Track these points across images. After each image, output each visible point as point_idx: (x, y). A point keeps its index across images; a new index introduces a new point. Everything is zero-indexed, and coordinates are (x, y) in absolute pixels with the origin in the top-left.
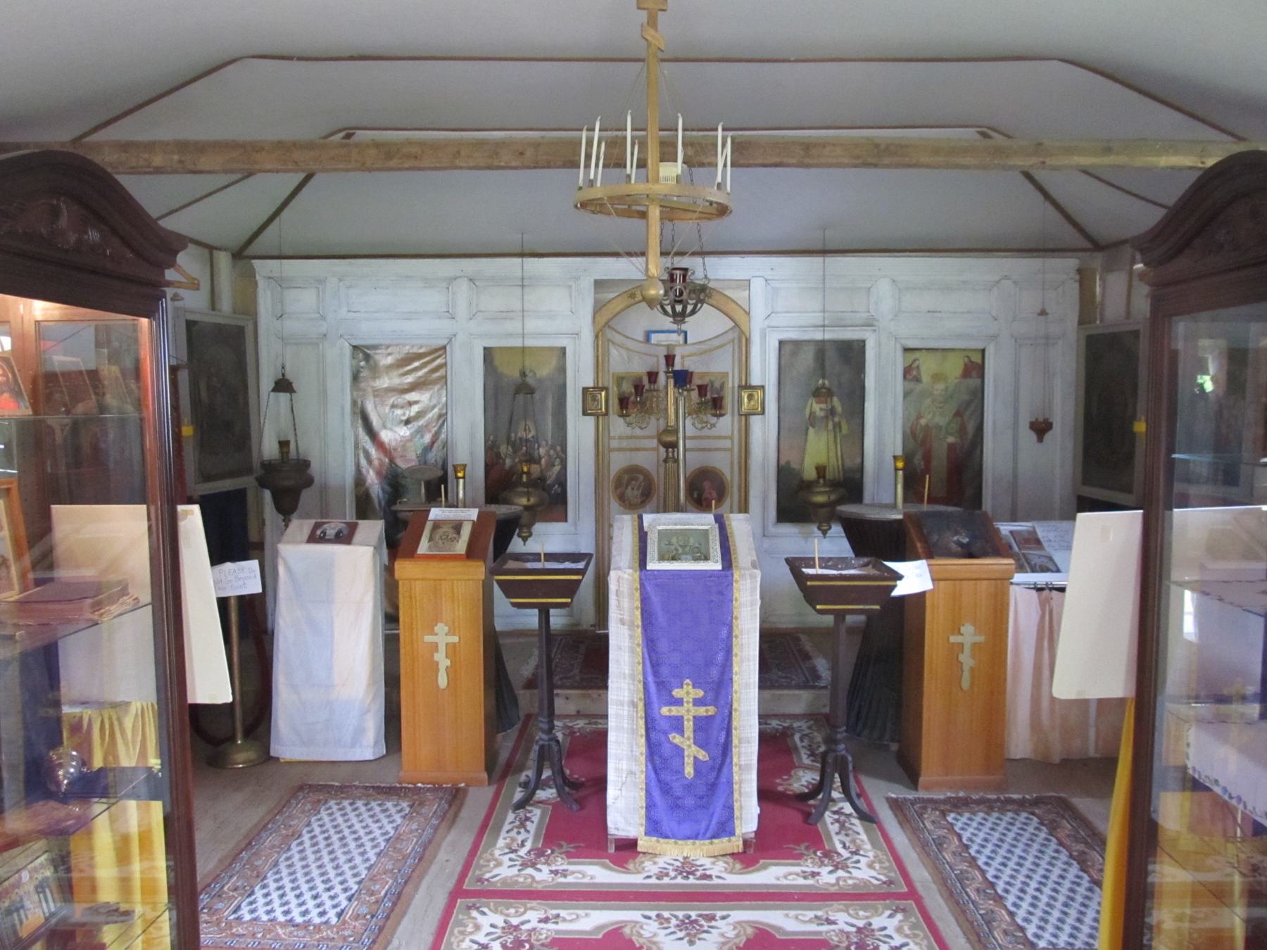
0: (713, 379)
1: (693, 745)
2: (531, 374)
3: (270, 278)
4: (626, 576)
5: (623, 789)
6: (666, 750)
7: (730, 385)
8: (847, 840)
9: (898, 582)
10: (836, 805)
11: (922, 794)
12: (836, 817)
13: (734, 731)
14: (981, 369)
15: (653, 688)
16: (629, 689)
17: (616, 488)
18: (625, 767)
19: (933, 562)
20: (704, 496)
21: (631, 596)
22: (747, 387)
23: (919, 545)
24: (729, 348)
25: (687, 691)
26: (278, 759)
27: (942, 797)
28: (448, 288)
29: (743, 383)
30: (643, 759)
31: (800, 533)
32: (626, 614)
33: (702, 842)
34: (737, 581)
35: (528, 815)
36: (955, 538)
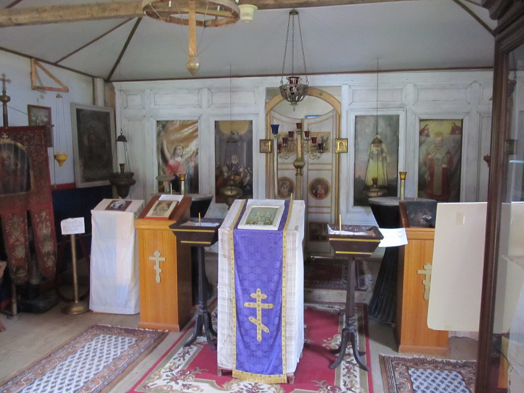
0: (323, 135)
1: (261, 324)
2: (236, 134)
3: (121, 90)
4: (226, 232)
5: (225, 344)
6: (247, 326)
7: (331, 138)
8: (348, 380)
9: (381, 240)
10: (350, 358)
11: (400, 355)
12: (348, 365)
13: (282, 318)
14: (461, 129)
15: (240, 292)
16: (228, 292)
17: (312, 191)
18: (226, 333)
19: (408, 229)
20: (318, 192)
21: (229, 243)
22: (339, 139)
23: (403, 219)
24: (331, 120)
25: (259, 295)
26: (92, 311)
27: (410, 358)
28: (199, 93)
29: (338, 137)
30: (235, 329)
31: (365, 211)
32: (227, 252)
33: (265, 375)
34: (285, 237)
35: (189, 350)
36: (424, 216)
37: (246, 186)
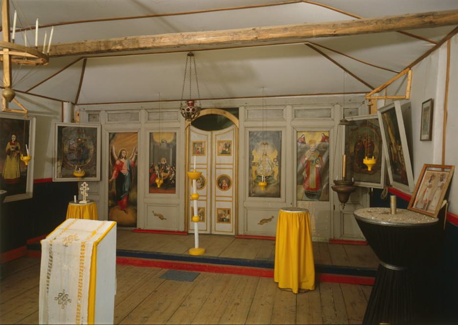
17: (219, 184)
20: (223, 185)
24: (232, 132)
37: (171, 181)
